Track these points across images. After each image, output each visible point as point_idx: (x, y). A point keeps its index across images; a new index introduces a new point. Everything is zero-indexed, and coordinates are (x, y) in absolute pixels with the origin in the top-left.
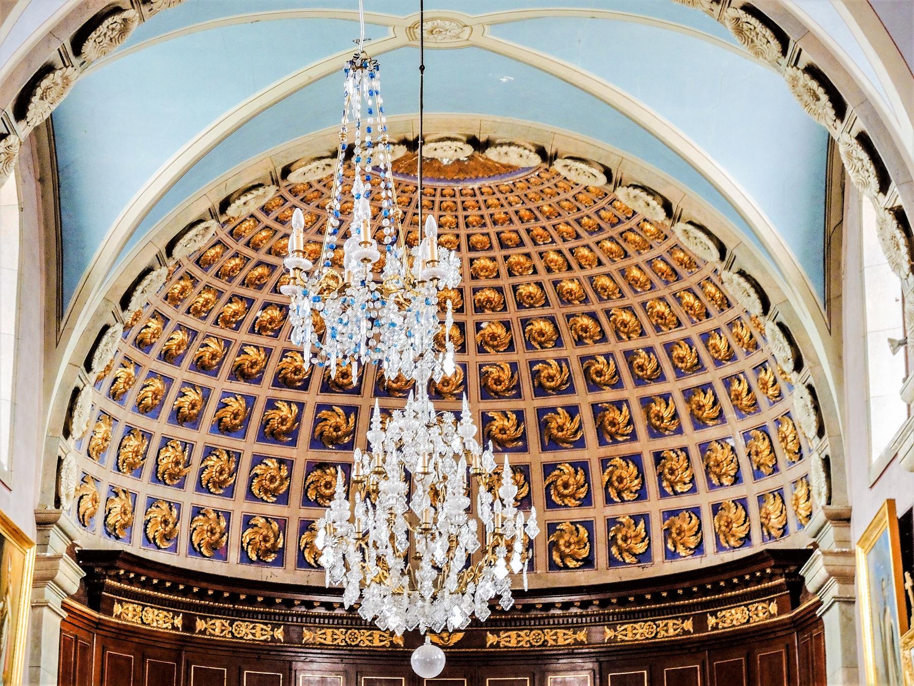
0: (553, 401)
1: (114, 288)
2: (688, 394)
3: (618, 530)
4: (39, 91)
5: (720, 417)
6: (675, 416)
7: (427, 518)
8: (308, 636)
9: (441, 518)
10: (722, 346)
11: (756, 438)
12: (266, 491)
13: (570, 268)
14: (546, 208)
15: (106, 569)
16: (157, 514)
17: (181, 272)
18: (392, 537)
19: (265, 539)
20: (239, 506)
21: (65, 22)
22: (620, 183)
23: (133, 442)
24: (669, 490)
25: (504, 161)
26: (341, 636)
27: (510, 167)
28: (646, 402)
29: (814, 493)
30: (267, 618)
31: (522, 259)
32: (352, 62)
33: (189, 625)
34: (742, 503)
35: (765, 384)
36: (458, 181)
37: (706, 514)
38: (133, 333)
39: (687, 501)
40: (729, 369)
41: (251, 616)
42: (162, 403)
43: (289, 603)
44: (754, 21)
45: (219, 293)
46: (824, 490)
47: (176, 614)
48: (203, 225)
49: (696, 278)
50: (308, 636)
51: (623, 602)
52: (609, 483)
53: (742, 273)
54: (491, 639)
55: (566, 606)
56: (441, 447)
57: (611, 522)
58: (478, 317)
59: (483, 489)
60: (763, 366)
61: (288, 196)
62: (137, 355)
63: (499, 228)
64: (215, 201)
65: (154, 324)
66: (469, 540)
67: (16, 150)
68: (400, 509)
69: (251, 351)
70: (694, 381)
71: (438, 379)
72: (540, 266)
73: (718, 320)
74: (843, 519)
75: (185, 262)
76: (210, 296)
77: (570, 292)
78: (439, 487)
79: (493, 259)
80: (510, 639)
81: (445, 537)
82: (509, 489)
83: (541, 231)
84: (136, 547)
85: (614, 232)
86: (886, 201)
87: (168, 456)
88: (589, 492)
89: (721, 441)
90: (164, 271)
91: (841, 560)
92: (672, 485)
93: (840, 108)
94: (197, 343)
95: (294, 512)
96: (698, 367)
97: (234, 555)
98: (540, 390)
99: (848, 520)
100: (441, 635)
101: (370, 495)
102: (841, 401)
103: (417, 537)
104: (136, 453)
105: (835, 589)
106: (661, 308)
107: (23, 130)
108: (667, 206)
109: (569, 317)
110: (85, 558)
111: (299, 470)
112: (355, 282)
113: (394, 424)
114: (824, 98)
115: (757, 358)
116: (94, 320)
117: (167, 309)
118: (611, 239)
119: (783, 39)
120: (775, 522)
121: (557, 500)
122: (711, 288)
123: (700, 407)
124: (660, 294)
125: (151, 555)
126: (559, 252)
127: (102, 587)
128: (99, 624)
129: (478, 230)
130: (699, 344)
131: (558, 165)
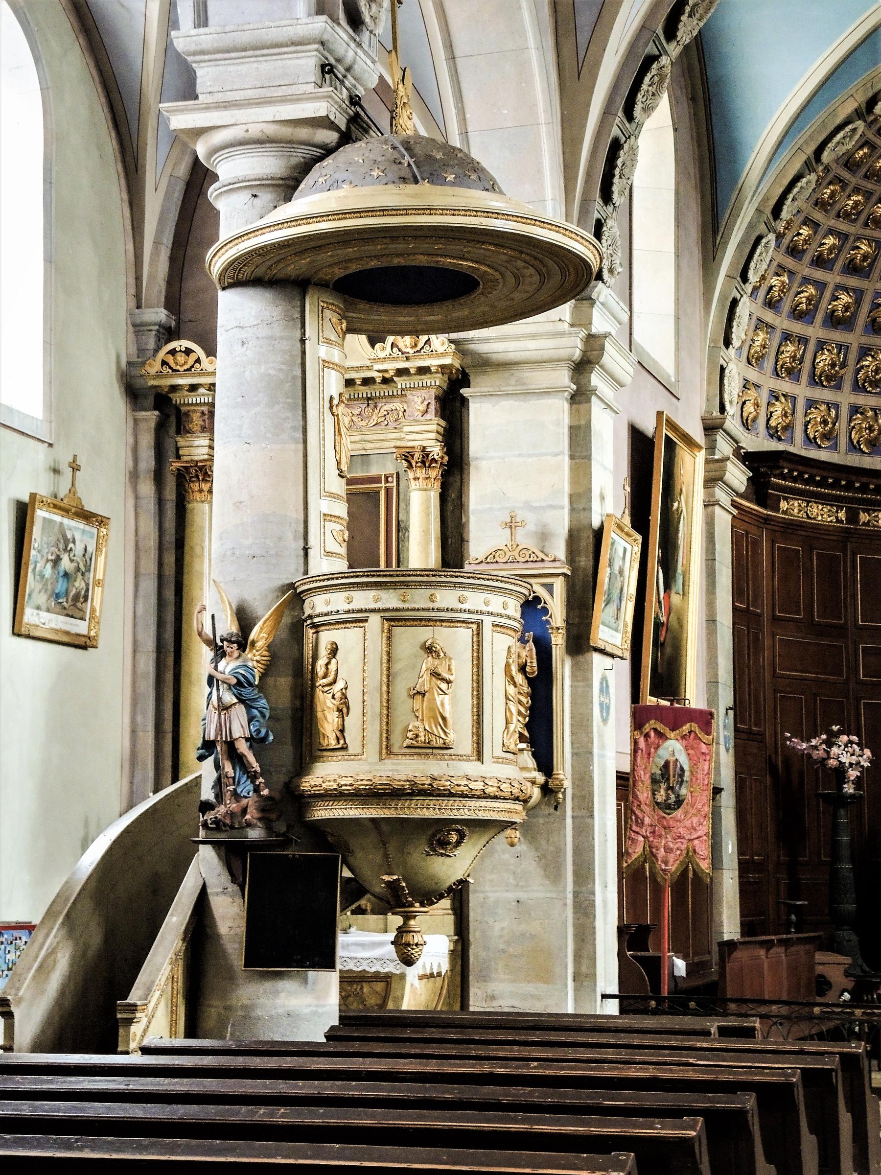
1: (765, 199)
16: (816, 415)
17: (830, 176)
23: (790, 348)
33: (853, 517)
38: (786, 241)
65: (805, 231)
67: (668, 70)
84: (798, 448)
87: (824, 359)
90: (813, 177)
94: (848, 246)
104: (794, 358)
107: (674, 50)
110: (749, 459)
117: (818, 216)
125: (813, 454)
128: (767, 520)
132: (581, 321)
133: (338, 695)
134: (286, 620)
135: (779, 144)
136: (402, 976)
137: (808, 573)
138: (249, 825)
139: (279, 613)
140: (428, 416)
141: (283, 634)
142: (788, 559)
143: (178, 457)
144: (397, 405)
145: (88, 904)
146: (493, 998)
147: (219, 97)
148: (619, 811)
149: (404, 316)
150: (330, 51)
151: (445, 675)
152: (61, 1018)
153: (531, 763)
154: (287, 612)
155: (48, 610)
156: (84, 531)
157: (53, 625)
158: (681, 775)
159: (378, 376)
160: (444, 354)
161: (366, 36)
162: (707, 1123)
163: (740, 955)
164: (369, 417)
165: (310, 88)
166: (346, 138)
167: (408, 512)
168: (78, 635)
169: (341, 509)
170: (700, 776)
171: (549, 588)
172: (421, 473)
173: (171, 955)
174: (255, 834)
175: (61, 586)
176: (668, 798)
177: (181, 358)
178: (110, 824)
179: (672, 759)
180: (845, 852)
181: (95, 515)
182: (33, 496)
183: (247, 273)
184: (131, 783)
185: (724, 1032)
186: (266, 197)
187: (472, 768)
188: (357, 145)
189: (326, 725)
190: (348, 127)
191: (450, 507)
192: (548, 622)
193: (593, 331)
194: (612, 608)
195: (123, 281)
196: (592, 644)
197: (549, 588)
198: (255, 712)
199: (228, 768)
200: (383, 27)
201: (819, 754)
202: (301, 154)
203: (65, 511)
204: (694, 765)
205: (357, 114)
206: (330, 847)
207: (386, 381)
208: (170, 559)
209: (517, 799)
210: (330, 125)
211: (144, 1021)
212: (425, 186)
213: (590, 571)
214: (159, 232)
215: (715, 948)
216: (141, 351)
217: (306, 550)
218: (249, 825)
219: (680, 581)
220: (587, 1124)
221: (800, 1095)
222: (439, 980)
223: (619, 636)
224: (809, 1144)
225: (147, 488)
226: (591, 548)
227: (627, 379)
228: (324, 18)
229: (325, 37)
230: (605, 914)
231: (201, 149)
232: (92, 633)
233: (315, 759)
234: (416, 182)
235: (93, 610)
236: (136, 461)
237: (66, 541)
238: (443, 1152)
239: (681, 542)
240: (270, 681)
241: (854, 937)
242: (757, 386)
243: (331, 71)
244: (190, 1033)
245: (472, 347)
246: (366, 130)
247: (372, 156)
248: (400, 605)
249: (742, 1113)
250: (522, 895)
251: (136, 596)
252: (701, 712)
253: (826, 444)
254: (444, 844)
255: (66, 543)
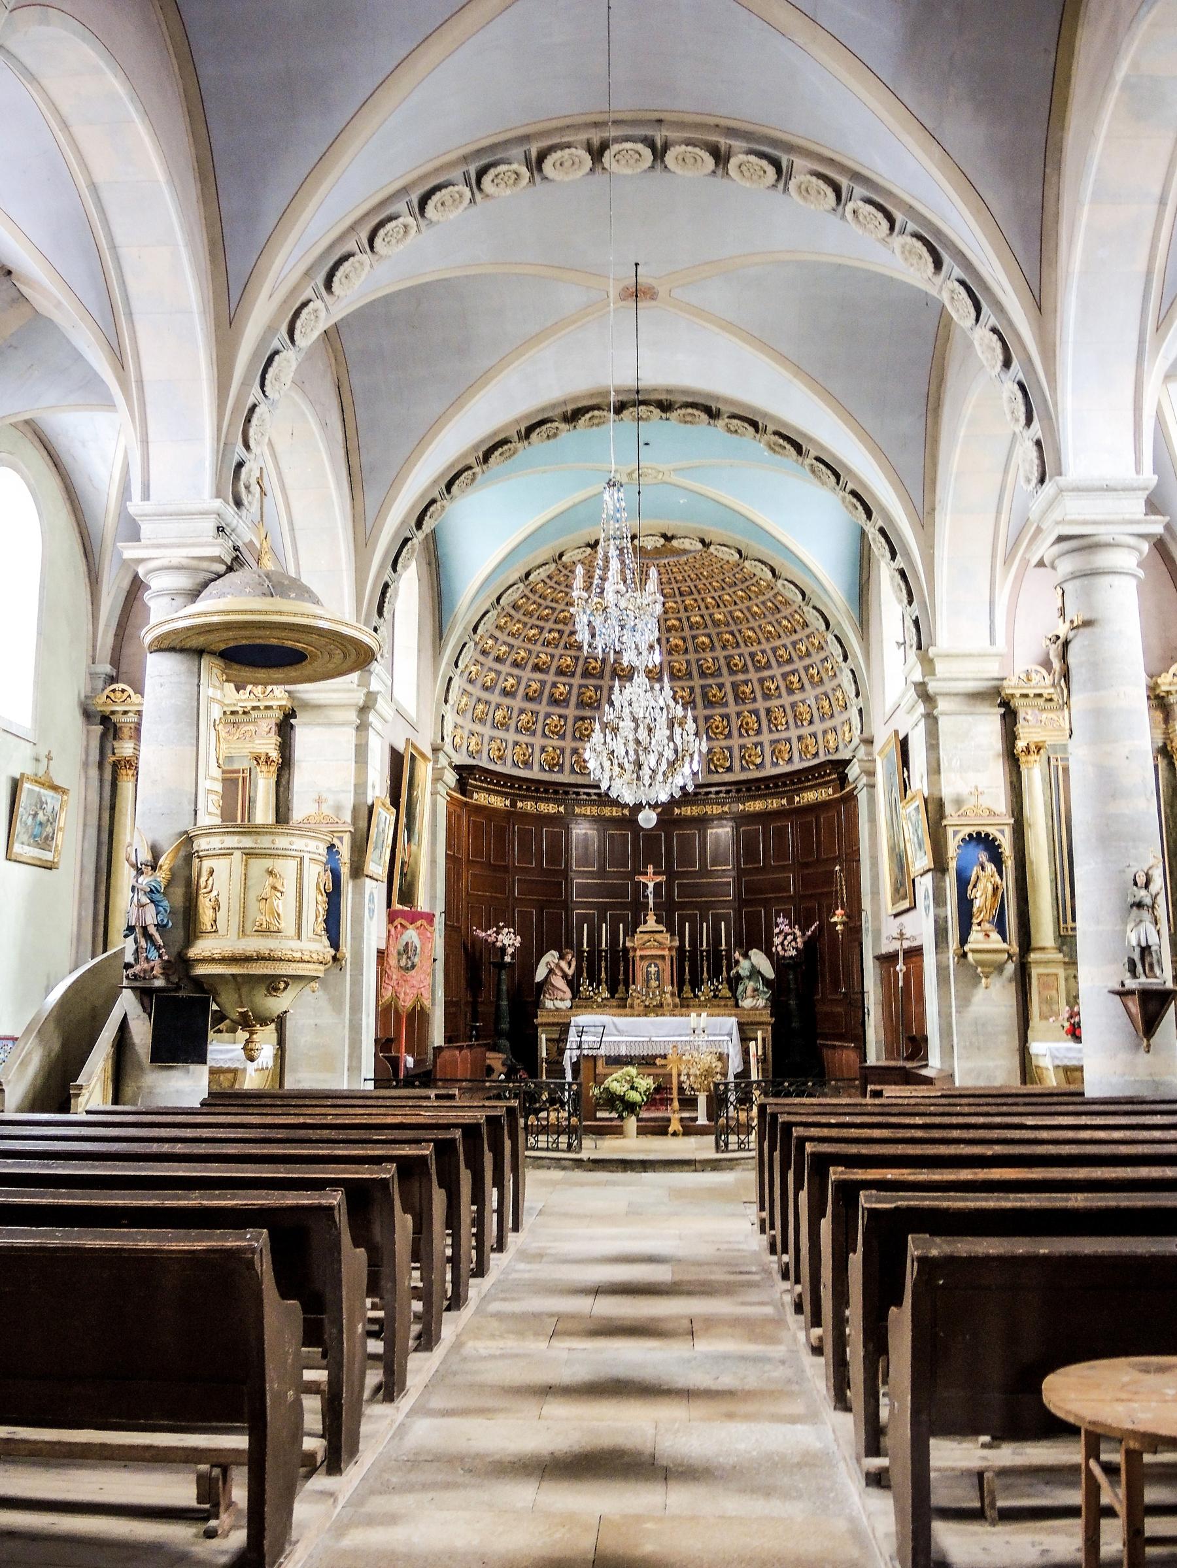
0: (710, 681)
1: (469, 622)
2: (785, 676)
3: (746, 751)
4: (429, 514)
5: (802, 688)
6: (777, 688)
7: (645, 742)
8: (577, 810)
9: (653, 741)
10: (804, 649)
11: (822, 699)
12: (553, 733)
13: (719, 606)
14: (705, 573)
15: (469, 774)
16: (494, 745)
17: (504, 613)
18: (627, 753)
19: (553, 759)
20: (538, 741)
21: (442, 475)
22: (746, 558)
23: (481, 707)
24: (774, 729)
25: (682, 547)
26: (595, 810)
27: (685, 550)
28: (761, 681)
29: (853, 728)
30: (555, 801)
31: (692, 602)
32: (608, 483)
33: (513, 804)
34: (814, 735)
35: (827, 670)
36: (656, 559)
37: (794, 741)
38: (480, 647)
39: (784, 735)
40: (807, 661)
41: (547, 800)
42: (496, 686)
43: (566, 793)
44: (821, 466)
45: (525, 624)
46: (859, 726)
47: (507, 799)
48: (516, 586)
49: (789, 611)
50: (577, 810)
51: (749, 790)
52: (741, 725)
53: (814, 608)
54: (677, 811)
55: (717, 793)
56: (653, 703)
57: (742, 747)
58: (668, 635)
59: (676, 725)
60: (826, 659)
61: (562, 569)
62: (481, 658)
63: (679, 585)
64: (523, 572)
65: (490, 642)
66: (669, 754)
67: (417, 546)
68: (631, 737)
69: (543, 656)
70: (788, 668)
71: (650, 666)
72: (703, 606)
73: (802, 634)
74: (869, 742)
75: (506, 607)
76: (520, 626)
77: (719, 620)
78: (652, 725)
79: (676, 602)
80: (687, 811)
81: (656, 752)
82: (690, 726)
83: (703, 586)
84: (484, 763)
85: (744, 586)
86: (894, 565)
87: (499, 714)
88: (730, 731)
89: (803, 702)
90: (495, 612)
91: (868, 764)
92: (776, 726)
93: (869, 513)
94: (513, 653)
95: (568, 744)
96: (790, 661)
97: (536, 767)
98: (703, 675)
99: (872, 742)
100: (654, 807)
101: (616, 730)
102: (869, 678)
103: (640, 753)
104: (483, 712)
105: (864, 780)
106: (770, 628)
107: (420, 535)
108: (773, 571)
109: (718, 634)
110: (458, 769)
111: (570, 722)
112: (611, 605)
113: (627, 691)
114: (860, 508)
115: (822, 655)
116: (458, 640)
117: (497, 634)
118: (742, 590)
119: (837, 476)
120: (832, 744)
121: (713, 736)
122: (797, 617)
123: (792, 683)
124: (769, 620)
125: (491, 767)
126: (713, 598)
127: (467, 784)
128: (466, 804)
129: (668, 586)
130: (790, 648)
131: (712, 549)
132: (363, 683)
133: (213, 899)
134: (182, 853)
135: (477, 592)
136: (245, 1070)
137: (488, 833)
138: (155, 977)
139: (178, 848)
140: (270, 735)
141: (180, 861)
142: (477, 830)
143: (114, 753)
144: (251, 727)
145: (51, 1026)
146: (299, 1082)
147: (155, 541)
148: (377, 972)
149: (262, 674)
150: (223, 520)
151: (280, 888)
152: (34, 1093)
153: (327, 943)
154: (182, 848)
155: (29, 845)
156: (53, 797)
157: (31, 854)
158: (415, 951)
159: (241, 711)
160: (281, 699)
161: (244, 512)
162: (435, 1146)
163: (446, 1054)
164: (234, 734)
165: (210, 539)
166: (230, 569)
167: (256, 792)
168: (46, 861)
169: (218, 787)
170: (426, 951)
171: (341, 839)
172: (265, 768)
173: (104, 1055)
174: (159, 983)
175: (37, 830)
176: (407, 964)
177: (119, 694)
178: (63, 978)
179: (410, 942)
180: (504, 996)
181: (60, 787)
182: (22, 775)
183: (165, 644)
184: (77, 952)
185: (438, 1097)
186: (180, 600)
187: (294, 944)
188: (237, 573)
189: (205, 917)
190: (232, 563)
191: (282, 789)
192: (339, 859)
193: (371, 690)
194: (378, 851)
195: (85, 647)
196: (365, 873)
197: (341, 839)
198: (161, 908)
199: (143, 943)
200: (255, 509)
201: (492, 939)
202: (202, 577)
203: (42, 784)
204: (423, 944)
205: (237, 556)
206: (204, 991)
207: (244, 713)
208: (106, 815)
209: (321, 963)
210: (222, 562)
211: (87, 1095)
212: (277, 599)
213: (365, 830)
214: (108, 620)
215: (430, 1051)
216: (93, 690)
217: (196, 811)
218: (155, 977)
219: (416, 836)
220: (366, 1149)
221: (484, 1131)
222: (267, 1072)
223: (381, 868)
224: (488, 1157)
225: (94, 772)
226: (366, 816)
227: (390, 718)
228: (220, 500)
229: (220, 511)
230: (368, 1032)
231: (141, 571)
232: (56, 860)
233: (197, 938)
234: (272, 596)
235: (57, 846)
236: (87, 755)
237: (42, 803)
238: (281, 1167)
239: (417, 815)
240: (171, 890)
241: (507, 1044)
242: (462, 727)
243: (223, 531)
244: (116, 1101)
245: (298, 695)
246: (242, 565)
247: (246, 580)
248: (254, 846)
249: (453, 1141)
250: (318, 1021)
251: (84, 837)
252: (428, 914)
253: (499, 762)
254: (276, 989)
255: (41, 804)
